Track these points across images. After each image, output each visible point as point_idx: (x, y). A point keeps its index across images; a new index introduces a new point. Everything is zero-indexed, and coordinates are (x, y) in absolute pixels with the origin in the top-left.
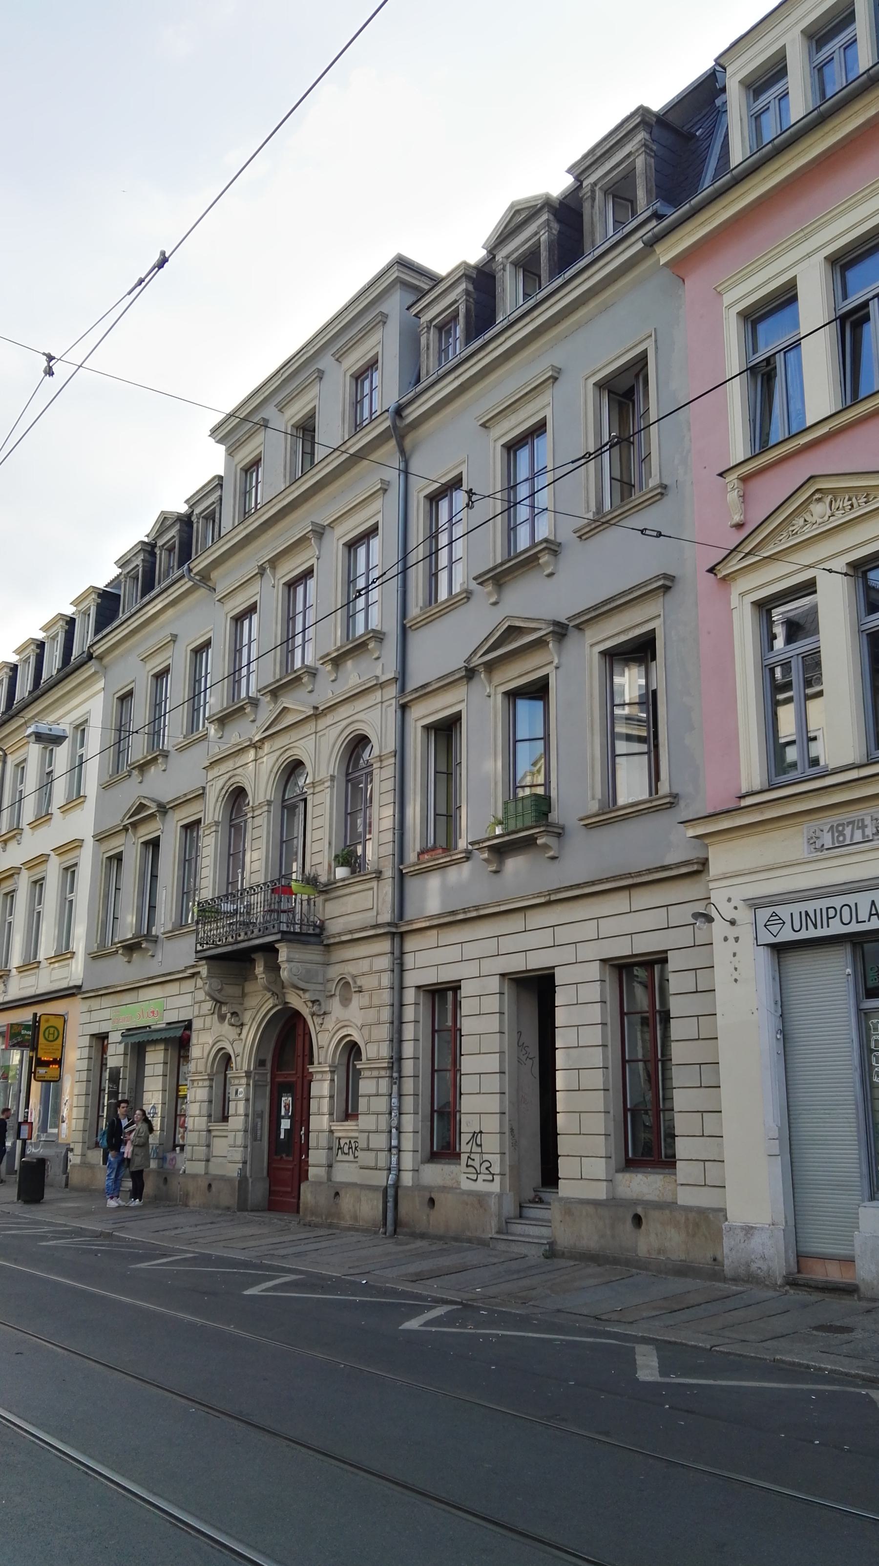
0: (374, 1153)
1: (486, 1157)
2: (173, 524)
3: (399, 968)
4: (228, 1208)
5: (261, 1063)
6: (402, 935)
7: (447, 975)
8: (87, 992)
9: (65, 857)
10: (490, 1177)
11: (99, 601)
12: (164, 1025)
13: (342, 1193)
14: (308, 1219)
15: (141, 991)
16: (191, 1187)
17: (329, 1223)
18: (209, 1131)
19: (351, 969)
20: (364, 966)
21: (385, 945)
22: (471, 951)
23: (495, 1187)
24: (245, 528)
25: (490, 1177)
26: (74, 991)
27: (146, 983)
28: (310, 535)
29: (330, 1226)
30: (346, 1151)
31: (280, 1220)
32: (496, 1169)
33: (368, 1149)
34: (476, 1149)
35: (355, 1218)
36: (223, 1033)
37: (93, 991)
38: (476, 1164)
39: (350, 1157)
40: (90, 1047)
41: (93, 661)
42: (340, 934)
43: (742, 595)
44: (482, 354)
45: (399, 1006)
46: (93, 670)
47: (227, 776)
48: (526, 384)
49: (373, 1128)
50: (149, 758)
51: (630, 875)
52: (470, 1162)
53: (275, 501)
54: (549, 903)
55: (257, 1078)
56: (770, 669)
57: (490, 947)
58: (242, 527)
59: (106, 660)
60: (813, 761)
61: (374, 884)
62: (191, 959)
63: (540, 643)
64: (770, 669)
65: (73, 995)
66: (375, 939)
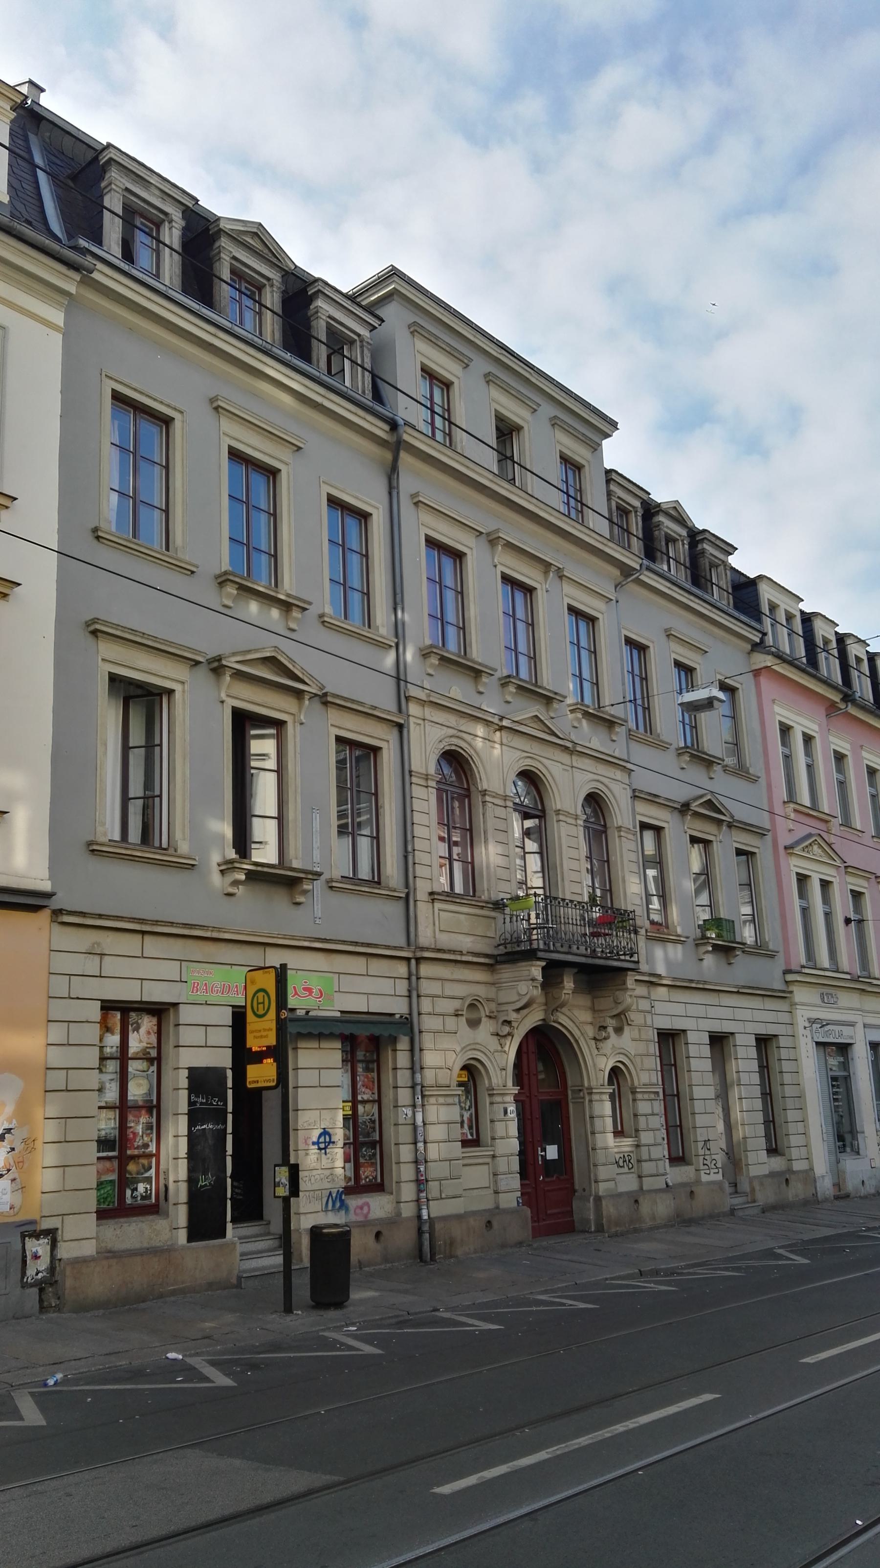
0: (654, 1163)
1: (714, 1157)
2: (26, 140)
4: (520, 1244)
6: (418, 960)
7: (678, 1024)
8: (643, 974)
10: (716, 1171)
12: (338, 1014)
13: (641, 1200)
14: (613, 1230)
15: (722, 995)
16: (457, 1231)
17: (632, 1229)
21: (401, 969)
22: (692, 1010)
23: (719, 1177)
24: (491, 481)
25: (716, 1171)
27: (306, 944)
29: (636, 1231)
30: (621, 1164)
31: (585, 1239)
32: (719, 1165)
33: (651, 1160)
34: (708, 1152)
35: (654, 1218)
36: (479, 1041)
37: (306, 939)
38: (708, 1162)
39: (626, 1170)
44: (686, 595)
47: (451, 732)
48: (692, 639)
49: (652, 1142)
50: (591, 711)
52: (705, 1162)
53: (534, 501)
54: (738, 992)
55: (581, 1094)
57: (700, 1011)
58: (491, 476)
63: (720, 822)
65: (36, 909)
66: (435, 962)
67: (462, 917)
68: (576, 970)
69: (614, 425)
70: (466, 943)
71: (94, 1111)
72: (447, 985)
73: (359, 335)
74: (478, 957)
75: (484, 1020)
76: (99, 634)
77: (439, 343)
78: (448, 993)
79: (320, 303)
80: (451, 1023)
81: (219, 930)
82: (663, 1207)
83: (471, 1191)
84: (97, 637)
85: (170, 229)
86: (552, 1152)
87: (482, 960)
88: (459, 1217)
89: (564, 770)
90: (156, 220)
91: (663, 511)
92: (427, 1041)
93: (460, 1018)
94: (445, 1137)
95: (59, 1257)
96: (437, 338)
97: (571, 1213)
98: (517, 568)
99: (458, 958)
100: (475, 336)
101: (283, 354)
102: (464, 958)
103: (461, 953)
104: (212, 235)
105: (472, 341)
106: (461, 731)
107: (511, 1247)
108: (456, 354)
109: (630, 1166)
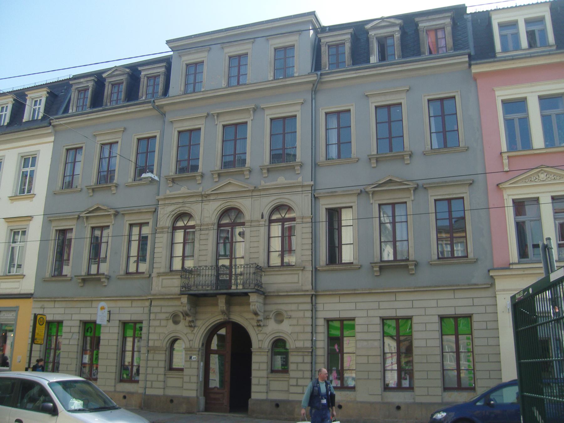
3: (314, 309)
5: (203, 345)
9: (11, 224)
11: (48, 95)
18: (165, 375)
19: (283, 307)
20: (294, 307)
26: (30, 296)
28: (251, 110)
40: (80, 326)
41: (51, 126)
42: (274, 292)
43: (509, 195)
45: (314, 326)
46: (50, 131)
51: (332, 291)
56: (25, 159)
59: (57, 128)
60: (143, 237)
61: (300, 272)
62: (177, 290)
64: (25, 159)
65: (30, 298)
75: (182, 321)
80: (164, 323)
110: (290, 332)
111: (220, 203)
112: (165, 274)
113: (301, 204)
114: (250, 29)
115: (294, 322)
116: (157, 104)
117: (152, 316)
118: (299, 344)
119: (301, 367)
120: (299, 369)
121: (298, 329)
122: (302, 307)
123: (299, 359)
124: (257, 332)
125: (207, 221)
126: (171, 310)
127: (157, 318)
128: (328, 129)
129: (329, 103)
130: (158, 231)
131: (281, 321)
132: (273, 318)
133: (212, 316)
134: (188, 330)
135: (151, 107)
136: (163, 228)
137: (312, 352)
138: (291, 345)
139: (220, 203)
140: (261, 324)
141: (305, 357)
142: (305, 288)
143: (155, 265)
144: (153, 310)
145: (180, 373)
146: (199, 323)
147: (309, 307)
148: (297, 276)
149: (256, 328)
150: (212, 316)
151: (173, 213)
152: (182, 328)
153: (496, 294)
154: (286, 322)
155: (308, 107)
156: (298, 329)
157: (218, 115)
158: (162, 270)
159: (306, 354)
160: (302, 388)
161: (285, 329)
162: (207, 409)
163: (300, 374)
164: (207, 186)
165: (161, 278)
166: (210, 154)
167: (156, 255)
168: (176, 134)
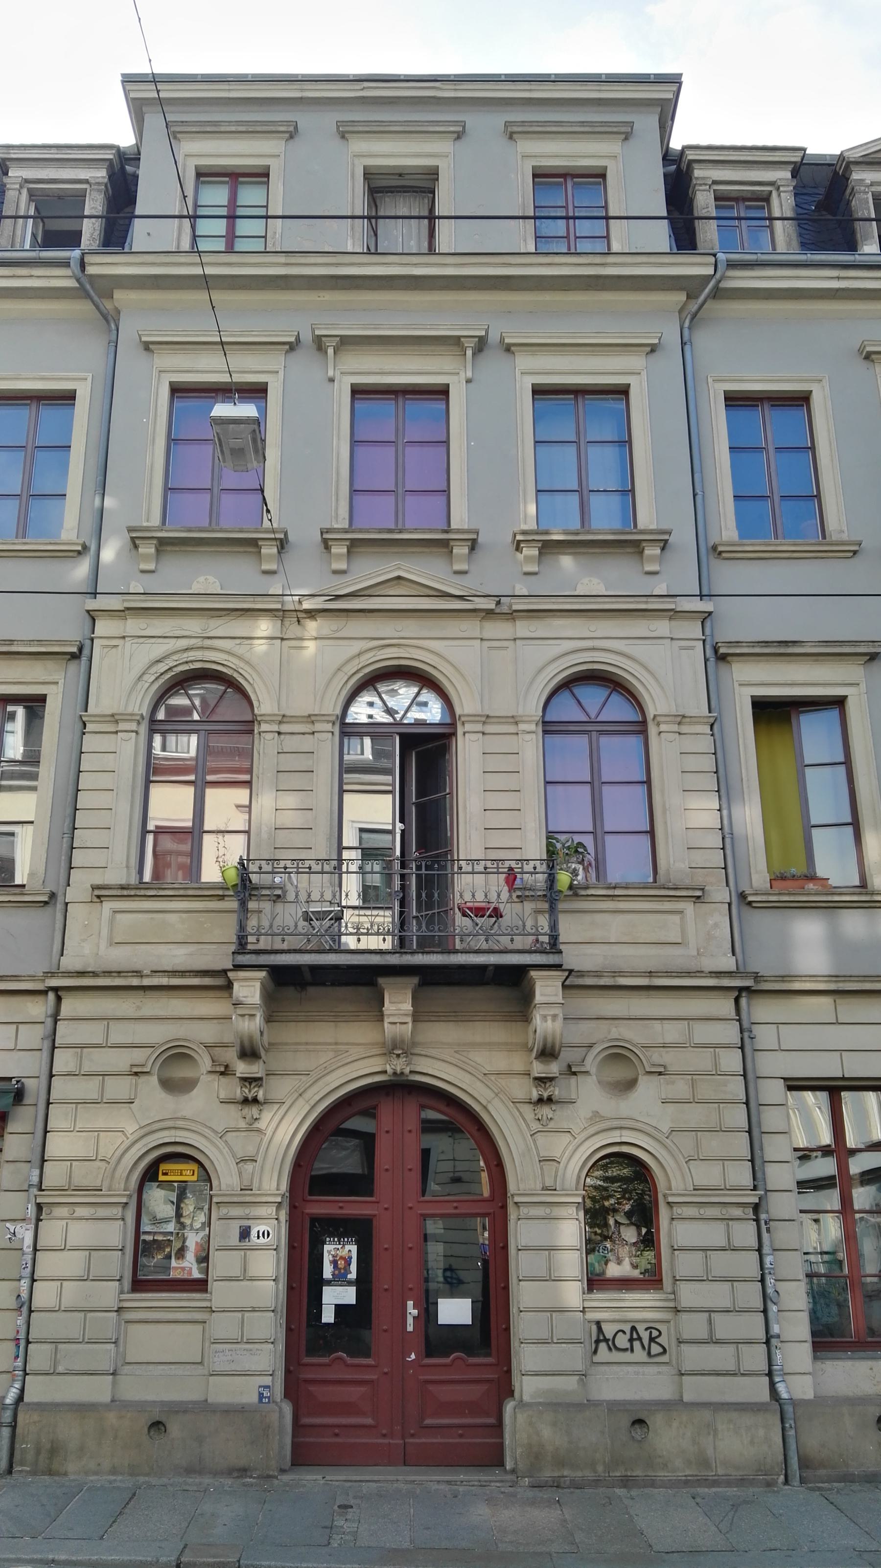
16: (69, 1431)
20: (672, 1033)
39: (639, 1354)
61: (688, 907)
67: (172, 918)
68: (415, 980)
69: (674, 81)
70: (179, 957)
71: (795, 1215)
72: (698, 1027)
73: (86, 181)
74: (174, 976)
75: (205, 1079)
76: (729, 658)
77: (223, 129)
78: (114, 1039)
79: (855, 176)
80: (119, 1088)
81: (15, 978)
82: (744, 1444)
83: (151, 1367)
84: (728, 662)
85: (779, 195)
86: (455, 1311)
87: (207, 981)
88: (82, 1409)
89: (682, 648)
90: (765, 195)
91: (857, 163)
92: (58, 1118)
93: (143, 1079)
94: (80, 1272)
95: (255, 1398)
96: (216, 123)
97: (498, 1426)
98: (387, 368)
99: (135, 982)
100: (302, 90)
101: (803, 257)
102: (146, 982)
103: (138, 973)
104: (843, 175)
105: (301, 98)
106: (209, 638)
107: (215, 1473)
108: (259, 129)
109: (656, 1349)
110: (665, 1128)
111: (357, 647)
112: (124, 891)
113: (665, 670)
114: (448, 92)
115: (681, 1088)
116: (91, 270)
117: (63, 1061)
118: (707, 1175)
119: (722, 1264)
120: (716, 1272)
121: (695, 1116)
122: (705, 1033)
123: (714, 1234)
124: (535, 1126)
125: (302, 705)
126: (159, 1034)
127: (86, 1068)
128: (36, 1281)
129: (747, 354)
130: (90, 727)
131: (630, 1085)
132: (593, 1070)
133: (336, 1058)
134: (234, 1116)
135: (72, 283)
136: (114, 718)
137: (756, 1208)
138: (673, 1177)
139: (357, 647)
140: (556, 1092)
141: (735, 1226)
142: (709, 964)
143: (79, 858)
144: (65, 1033)
145: (193, 1299)
146: (280, 1088)
147: (730, 1033)
148: (676, 918)
149: (528, 1110)
150: (336, 1058)
151: (162, 667)
152: (203, 1113)
153: (294, 1387)
154: (648, 1090)
155: (670, 363)
156: (695, 1116)
157: (345, 342)
158: (116, 876)
159: (737, 1212)
160: (731, 1348)
161: (646, 1119)
162: (303, 1456)
163: (717, 1295)
164: (303, 581)
165: (108, 906)
166: (307, 462)
167: (81, 819)
168: (165, 392)
